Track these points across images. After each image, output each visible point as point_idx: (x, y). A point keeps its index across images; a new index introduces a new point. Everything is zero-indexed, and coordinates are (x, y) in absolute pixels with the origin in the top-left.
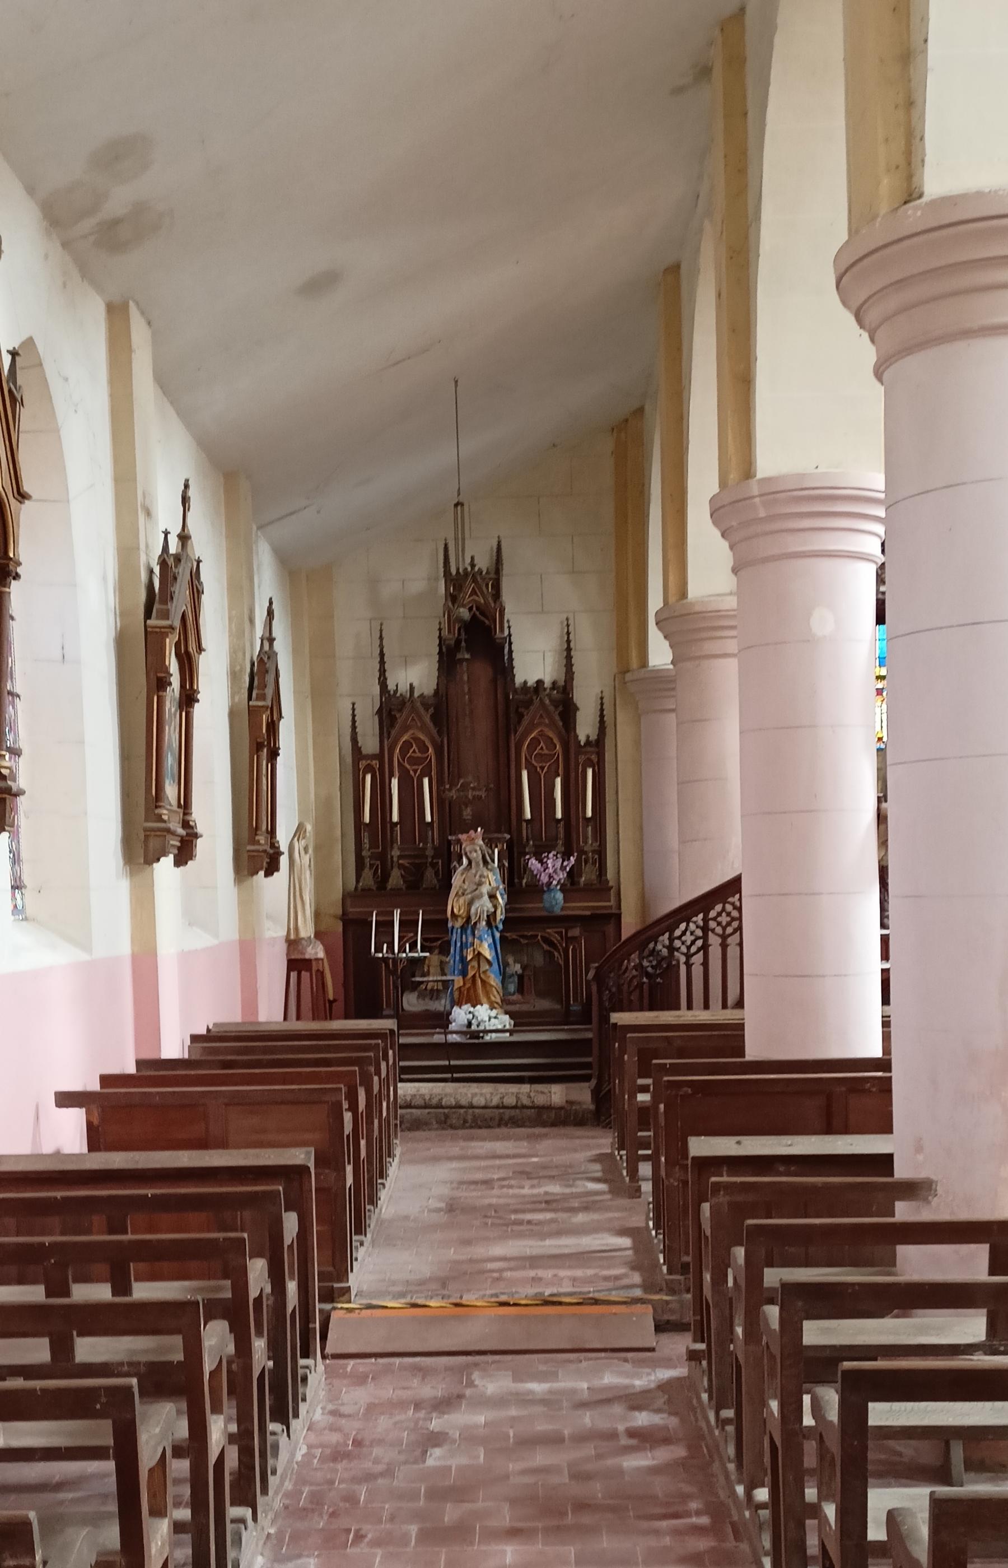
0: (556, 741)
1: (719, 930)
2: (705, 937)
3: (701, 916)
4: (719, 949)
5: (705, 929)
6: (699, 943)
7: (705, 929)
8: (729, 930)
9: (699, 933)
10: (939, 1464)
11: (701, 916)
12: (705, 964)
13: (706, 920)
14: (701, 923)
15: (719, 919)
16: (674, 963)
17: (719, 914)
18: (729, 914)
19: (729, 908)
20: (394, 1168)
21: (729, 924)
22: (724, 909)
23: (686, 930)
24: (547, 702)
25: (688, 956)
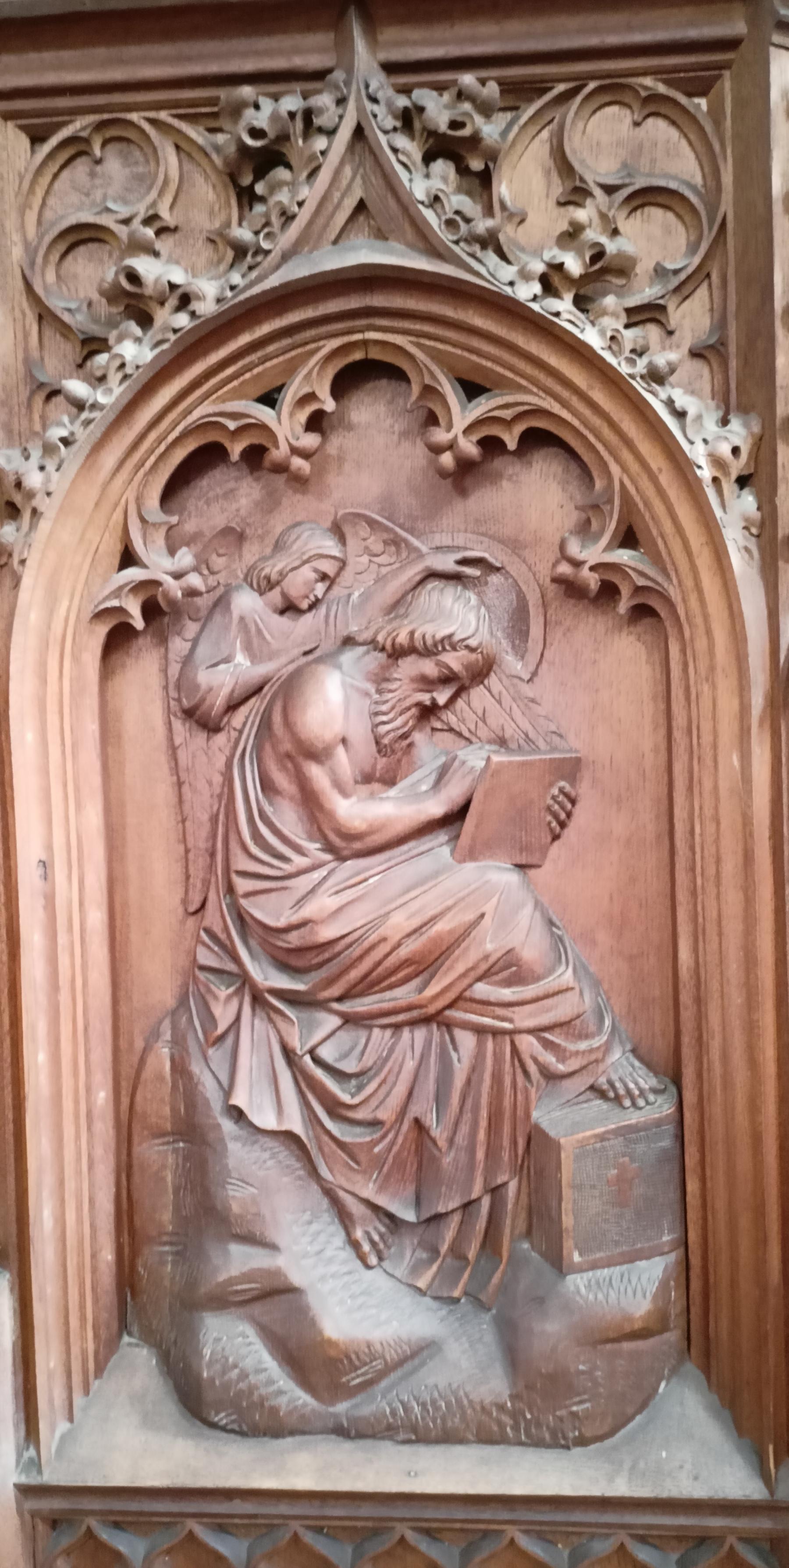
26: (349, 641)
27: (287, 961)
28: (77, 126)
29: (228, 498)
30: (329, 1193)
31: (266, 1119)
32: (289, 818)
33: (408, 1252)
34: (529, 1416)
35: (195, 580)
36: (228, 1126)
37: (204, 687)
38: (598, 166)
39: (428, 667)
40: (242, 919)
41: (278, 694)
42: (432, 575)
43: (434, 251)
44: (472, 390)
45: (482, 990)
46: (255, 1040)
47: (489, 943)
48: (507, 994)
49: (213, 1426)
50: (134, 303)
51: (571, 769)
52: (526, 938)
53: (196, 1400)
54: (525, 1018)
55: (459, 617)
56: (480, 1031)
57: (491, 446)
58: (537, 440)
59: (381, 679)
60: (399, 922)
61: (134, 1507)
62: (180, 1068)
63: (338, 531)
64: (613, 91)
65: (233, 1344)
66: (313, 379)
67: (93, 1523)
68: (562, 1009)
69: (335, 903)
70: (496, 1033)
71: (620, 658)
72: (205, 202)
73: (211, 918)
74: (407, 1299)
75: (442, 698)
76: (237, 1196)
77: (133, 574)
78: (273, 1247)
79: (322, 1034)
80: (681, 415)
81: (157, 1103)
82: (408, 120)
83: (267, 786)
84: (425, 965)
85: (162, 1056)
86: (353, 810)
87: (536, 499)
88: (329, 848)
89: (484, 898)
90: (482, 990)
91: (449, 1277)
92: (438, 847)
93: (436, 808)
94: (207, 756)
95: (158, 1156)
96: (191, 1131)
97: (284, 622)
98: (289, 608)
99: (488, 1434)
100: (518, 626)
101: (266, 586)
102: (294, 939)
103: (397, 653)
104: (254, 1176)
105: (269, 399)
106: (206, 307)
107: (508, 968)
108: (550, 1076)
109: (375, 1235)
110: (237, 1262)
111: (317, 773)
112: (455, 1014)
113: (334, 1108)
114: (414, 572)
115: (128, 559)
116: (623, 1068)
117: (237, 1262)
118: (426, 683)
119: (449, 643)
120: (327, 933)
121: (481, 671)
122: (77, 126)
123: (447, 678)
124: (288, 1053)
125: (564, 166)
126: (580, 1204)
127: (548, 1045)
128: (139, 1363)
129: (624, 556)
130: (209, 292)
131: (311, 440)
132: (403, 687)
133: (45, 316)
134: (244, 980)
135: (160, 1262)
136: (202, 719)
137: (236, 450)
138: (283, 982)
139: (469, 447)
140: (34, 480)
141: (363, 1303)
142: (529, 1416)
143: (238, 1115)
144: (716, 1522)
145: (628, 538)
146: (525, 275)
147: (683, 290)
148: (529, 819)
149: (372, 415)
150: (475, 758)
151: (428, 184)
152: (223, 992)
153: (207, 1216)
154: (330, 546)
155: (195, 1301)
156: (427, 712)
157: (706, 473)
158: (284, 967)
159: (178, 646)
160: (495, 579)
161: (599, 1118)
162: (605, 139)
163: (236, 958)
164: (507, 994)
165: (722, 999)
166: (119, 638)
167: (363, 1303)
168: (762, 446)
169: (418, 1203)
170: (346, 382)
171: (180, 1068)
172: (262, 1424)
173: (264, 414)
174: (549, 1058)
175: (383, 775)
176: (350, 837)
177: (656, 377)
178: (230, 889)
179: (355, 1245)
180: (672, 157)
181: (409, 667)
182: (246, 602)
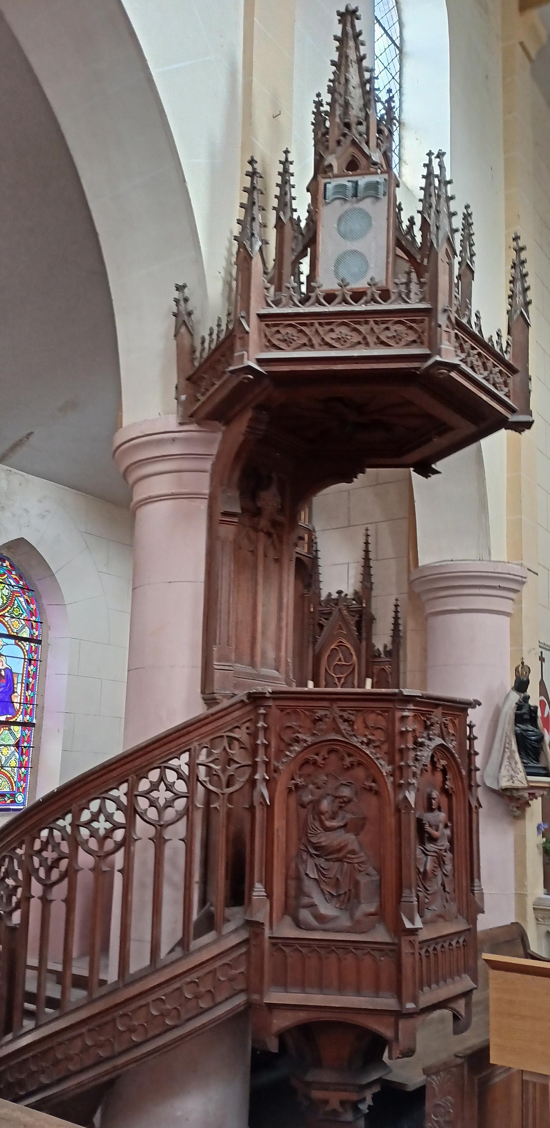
0: (353, 653)
1: (152, 814)
2: (129, 826)
3: (124, 788)
4: (63, 906)
5: (131, 811)
6: (119, 835)
7: (131, 811)
8: (170, 814)
9: (120, 817)
10: (286, 916)
11: (124, 788)
12: (127, 872)
13: (131, 795)
14: (185, 769)
15: (154, 794)
16: (105, 868)
17: (154, 786)
18: (109, 818)
19: (111, 806)
20: (417, 1036)
21: (169, 804)
22: (162, 778)
23: (100, 811)
24: (345, 612)
25: (160, 827)
26: (328, 794)
27: (316, 848)
28: (288, 711)
29: (309, 769)
30: (322, 890)
31: (312, 876)
32: (317, 824)
33: (335, 900)
34: (312, 610)
35: (304, 783)
36: (305, 877)
37: (418, 933)
38: (371, 724)
39: (341, 800)
40: (310, 842)
41: (316, 803)
42: (342, 784)
43: (345, 737)
44: (350, 755)
45: (349, 856)
46: (310, 863)
47: (350, 848)
48: (353, 856)
49: (302, 928)
50: (297, 740)
51: (364, 819)
52: (355, 846)
53: (298, 924)
54: (356, 861)
55: (346, 792)
56: (348, 863)
57: (352, 765)
58: (360, 764)
59: (333, 801)
60: (335, 843)
61: (287, 941)
62: (297, 867)
63: (327, 776)
64: (373, 712)
65: (305, 914)
66: (324, 753)
67: (280, 945)
68: (361, 860)
69: (324, 839)
70: (350, 863)
71: (373, 800)
72: (308, 723)
73: (303, 841)
74: (334, 909)
75: (343, 805)
76: (306, 889)
77: (293, 781)
78: (312, 898)
79: (321, 862)
80: (381, 765)
81: (292, 873)
82: (341, 717)
83: (314, 818)
84: (339, 850)
85: (293, 865)
86: (328, 824)
87: (360, 772)
88: (324, 830)
89: (349, 839)
90: (349, 856)
91: (341, 905)
92: (342, 831)
93: (342, 824)
94: (303, 812)
95: (292, 883)
96: (299, 879)
97: (317, 790)
98: (318, 788)
99: (348, 931)
100: (356, 793)
101: (314, 784)
102: (318, 845)
103: (336, 797)
104: (309, 886)
105: (317, 755)
106: (309, 743)
107: (353, 852)
108: (360, 871)
109: (330, 897)
110: (306, 900)
111: (322, 817)
112: (345, 860)
113: (324, 875)
114: (338, 783)
115: (293, 779)
116: (371, 870)
117: (306, 900)
118: (341, 803)
119: (345, 797)
120: (323, 844)
121: (350, 801)
122: (288, 711)
123: (344, 802)
124: (315, 864)
125: (365, 722)
126: (364, 892)
127: (359, 866)
128: (288, 919)
129: (373, 784)
130: (310, 739)
131: (323, 762)
132: (337, 803)
133: (282, 740)
134: (308, 852)
135: (292, 902)
136: (303, 806)
137: (311, 762)
138: (316, 853)
139: (349, 765)
140: (281, 768)
141: (326, 909)
142: (312, 610)
143: (307, 875)
144: (385, 947)
145: (374, 781)
146: (358, 742)
147: (383, 743)
148: (356, 827)
149: (333, 757)
150: (349, 816)
151: (344, 726)
152: (305, 854)
153: (301, 892)
154: (325, 778)
155: (299, 906)
156: (341, 808)
157: (385, 774)
158: (316, 850)
159: (299, 793)
160: (353, 786)
161: (367, 879)
162: (372, 719)
163: (307, 848)
164: (353, 856)
165: (103, 783)
166: (290, 791)
167: (326, 909)
168: (394, 770)
169: (337, 893)
170: (330, 751)
171: (297, 867)
172: (310, 928)
173: (316, 757)
174: (360, 868)
175: (333, 818)
176: (328, 828)
177: (378, 759)
178: (307, 836)
179: (326, 899)
180: (382, 723)
181: (338, 800)
182: (311, 786)
